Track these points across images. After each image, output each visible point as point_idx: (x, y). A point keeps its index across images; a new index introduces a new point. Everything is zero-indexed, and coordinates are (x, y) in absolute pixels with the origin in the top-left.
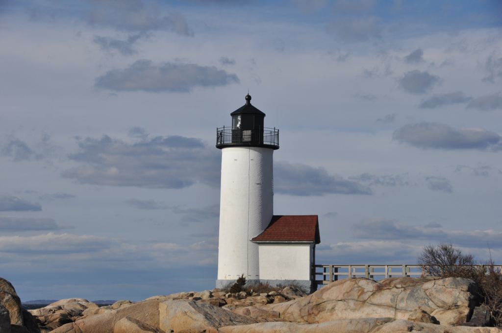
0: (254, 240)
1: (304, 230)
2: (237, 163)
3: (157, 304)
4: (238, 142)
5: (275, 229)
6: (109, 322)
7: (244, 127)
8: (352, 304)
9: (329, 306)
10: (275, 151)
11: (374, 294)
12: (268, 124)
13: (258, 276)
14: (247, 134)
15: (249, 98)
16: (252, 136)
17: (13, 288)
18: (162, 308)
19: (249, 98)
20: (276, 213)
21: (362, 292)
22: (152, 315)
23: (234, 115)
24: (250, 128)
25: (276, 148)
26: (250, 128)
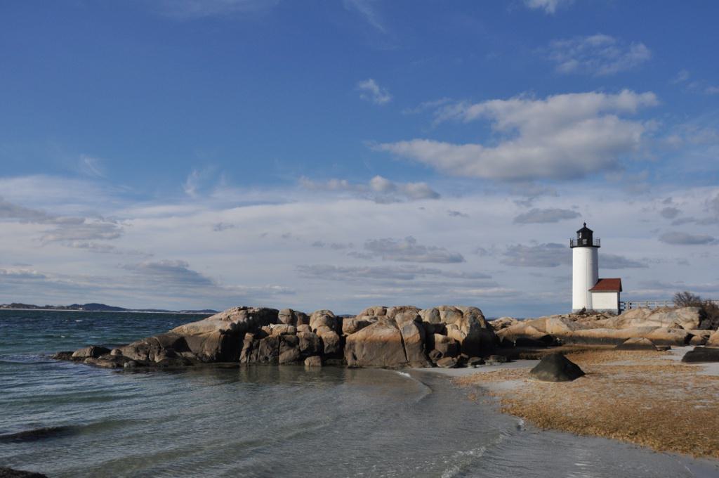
0: (590, 290)
1: (613, 285)
2: (580, 256)
3: (544, 320)
4: (580, 244)
5: (600, 285)
7: (583, 237)
8: (639, 320)
10: (599, 249)
12: (595, 236)
14: (585, 241)
15: (585, 224)
18: (547, 321)
19: (585, 224)
20: (600, 278)
21: (644, 314)
22: (543, 325)
23: (578, 232)
25: (599, 247)
26: (586, 237)
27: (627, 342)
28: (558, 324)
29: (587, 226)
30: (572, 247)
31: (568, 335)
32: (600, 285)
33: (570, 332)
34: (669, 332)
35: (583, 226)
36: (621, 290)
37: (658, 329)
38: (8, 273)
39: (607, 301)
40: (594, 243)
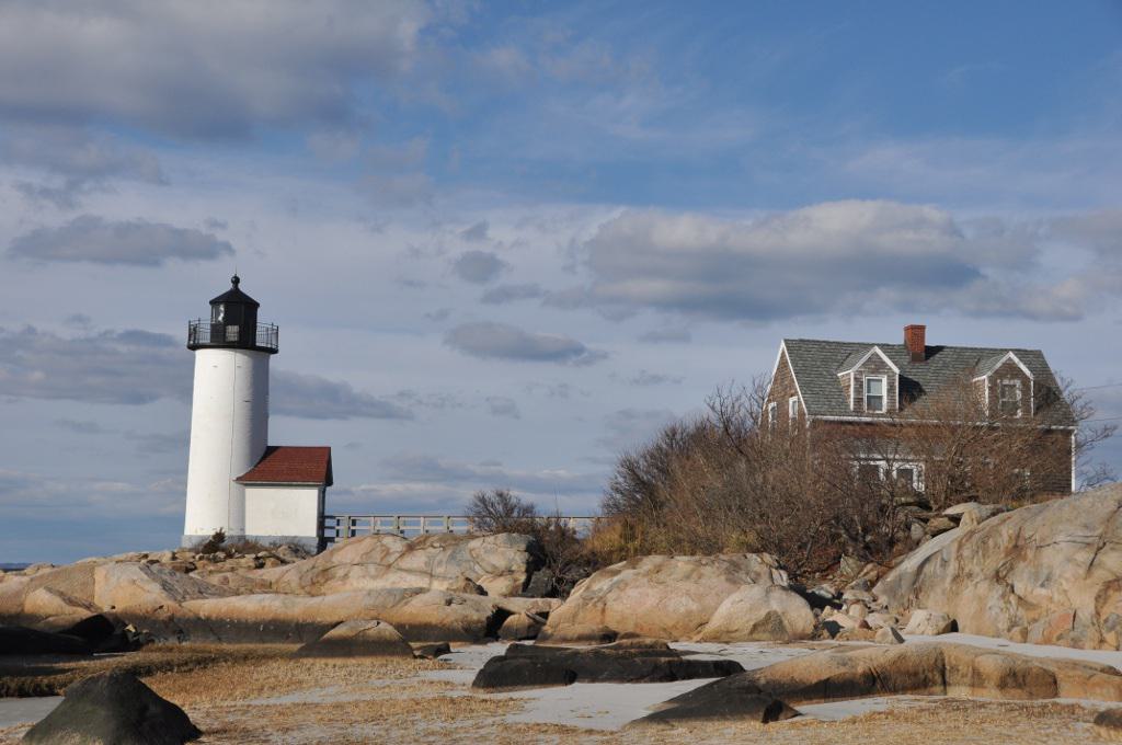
0: (239, 479)
1: (312, 467)
2: (216, 375)
4: (219, 341)
5: (269, 464)
6: (18, 594)
7: (228, 320)
8: (372, 569)
10: (272, 356)
11: (402, 555)
12: (264, 318)
13: (243, 530)
14: (233, 332)
15: (236, 281)
16: (241, 333)
18: (99, 574)
19: (236, 281)
20: (271, 443)
21: (387, 552)
23: (214, 303)
24: (237, 323)
25: (274, 351)
26: (237, 323)
27: (334, 633)
30: (194, 347)
31: (163, 615)
32: (269, 464)
33: (169, 603)
34: (449, 603)
35: (229, 286)
36: (329, 482)
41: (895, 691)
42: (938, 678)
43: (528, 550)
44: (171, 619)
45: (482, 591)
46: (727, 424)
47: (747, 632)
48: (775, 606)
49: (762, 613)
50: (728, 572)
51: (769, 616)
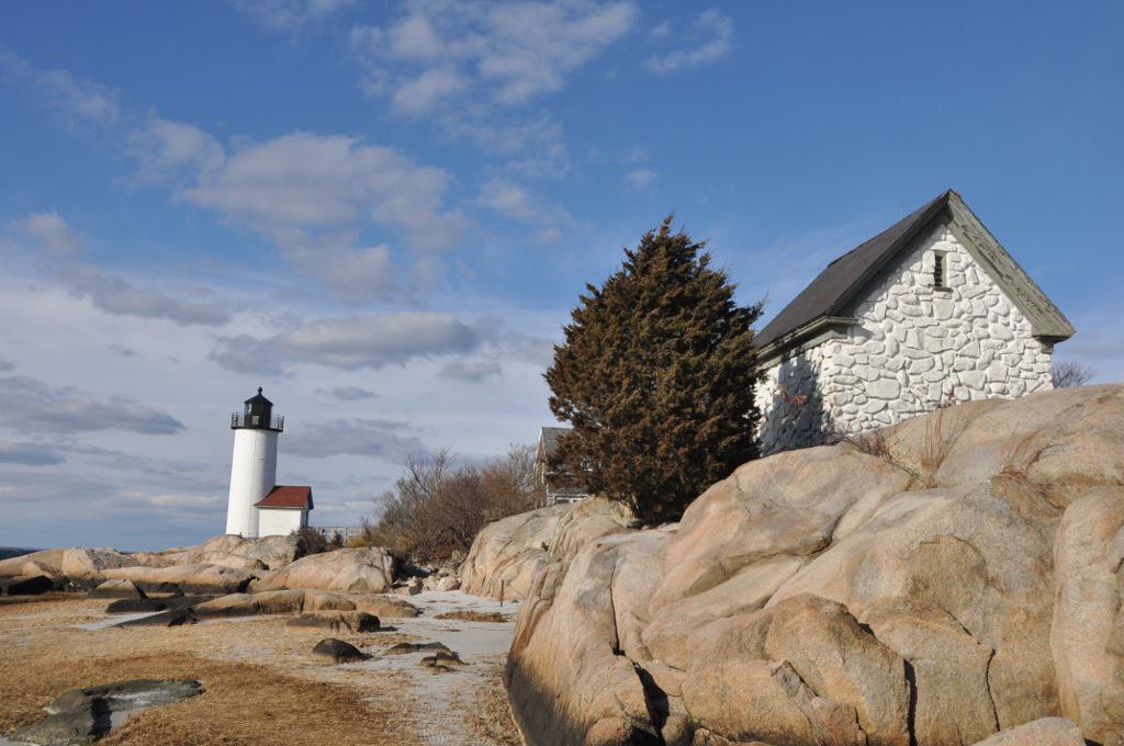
0: (256, 505)
1: (300, 498)
2: (247, 444)
3: (62, 552)
4: (248, 425)
5: (274, 495)
6: (20, 564)
7: (254, 413)
8: (221, 554)
9: (206, 557)
10: (280, 434)
11: (236, 547)
12: (275, 412)
13: (257, 534)
14: (256, 419)
15: (260, 390)
16: (260, 421)
17: (277, 536)
18: (66, 554)
19: (260, 390)
20: (277, 484)
21: (229, 546)
22: (57, 560)
23: (247, 403)
24: (260, 414)
25: (281, 431)
26: (260, 414)
27: (102, 586)
28: (80, 559)
29: (263, 394)
30: (234, 428)
31: (88, 577)
32: (274, 495)
33: (94, 571)
34: (222, 573)
35: (256, 393)
36: (311, 507)
37: (210, 569)
38: (429, 179)
39: (285, 522)
40: (274, 425)
41: (270, 613)
42: (298, 607)
43: (298, 545)
44: (93, 579)
45: (266, 568)
46: (498, 460)
47: (346, 588)
48: (363, 575)
49: (356, 579)
50: (357, 557)
51: (359, 580)
